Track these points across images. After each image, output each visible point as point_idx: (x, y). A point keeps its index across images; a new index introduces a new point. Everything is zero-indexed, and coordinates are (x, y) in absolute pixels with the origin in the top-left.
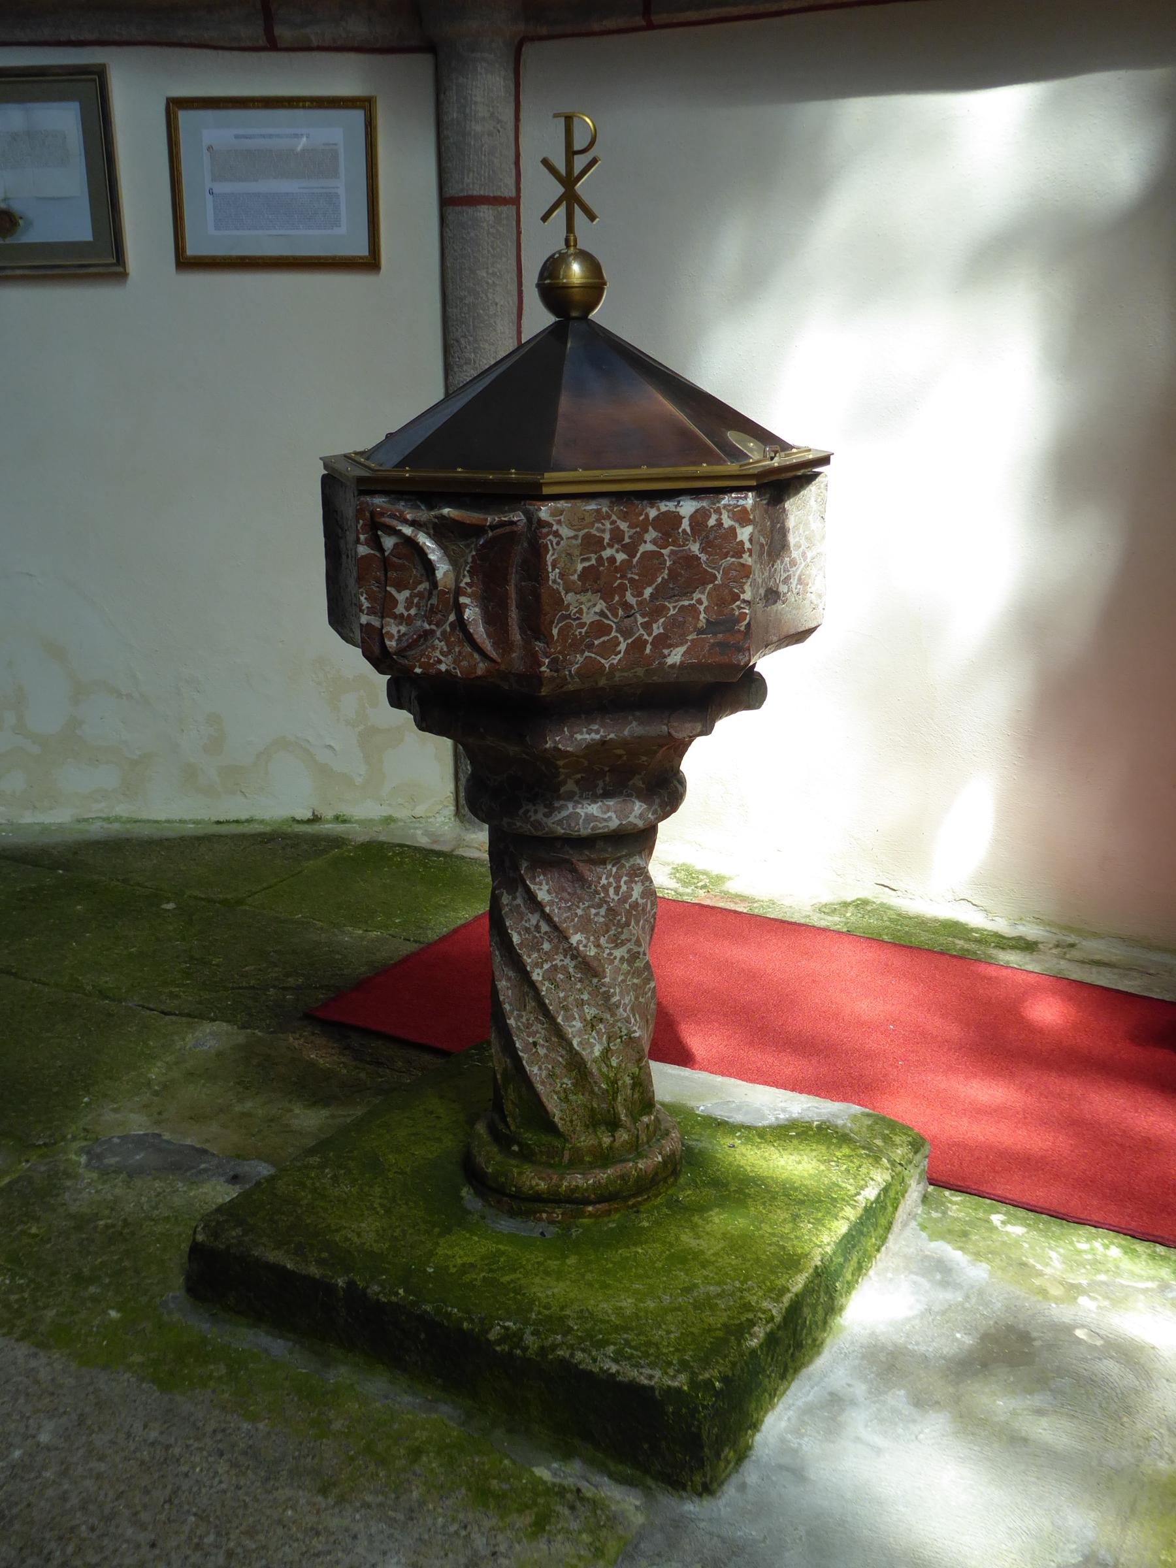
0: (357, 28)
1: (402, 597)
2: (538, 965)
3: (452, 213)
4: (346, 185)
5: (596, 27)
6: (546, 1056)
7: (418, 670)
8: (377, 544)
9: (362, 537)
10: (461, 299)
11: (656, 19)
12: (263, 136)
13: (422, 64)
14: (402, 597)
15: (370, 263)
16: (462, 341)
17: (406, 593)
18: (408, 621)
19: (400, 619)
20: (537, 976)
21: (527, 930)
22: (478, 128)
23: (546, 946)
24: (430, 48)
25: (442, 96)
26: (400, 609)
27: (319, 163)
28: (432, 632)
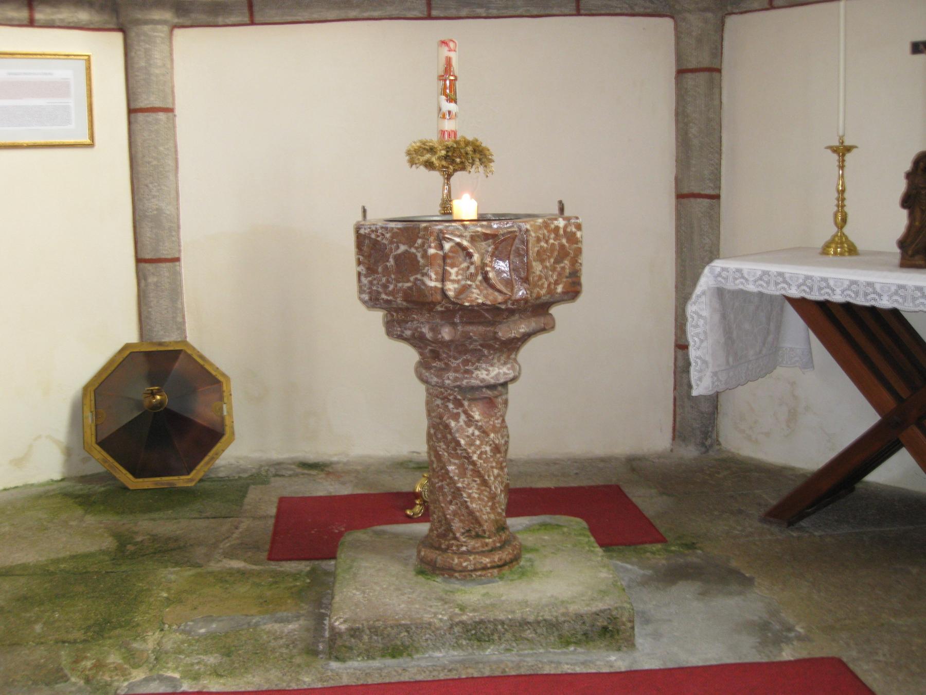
0: (83, 16)
1: (453, 271)
2: (474, 452)
3: (132, 115)
4: (76, 103)
5: (228, 21)
6: (479, 498)
7: (467, 304)
8: (441, 247)
9: (433, 245)
10: (149, 163)
11: (39, 16)
12: (25, 74)
13: (118, 37)
14: (453, 271)
15: (91, 145)
16: (150, 186)
17: (455, 269)
18: (458, 282)
19: (453, 281)
20: (475, 457)
21: (468, 436)
22: (157, 71)
23: (478, 442)
24: (121, 29)
25: (133, 54)
26: (453, 277)
27: (60, 89)
28: (470, 286)
